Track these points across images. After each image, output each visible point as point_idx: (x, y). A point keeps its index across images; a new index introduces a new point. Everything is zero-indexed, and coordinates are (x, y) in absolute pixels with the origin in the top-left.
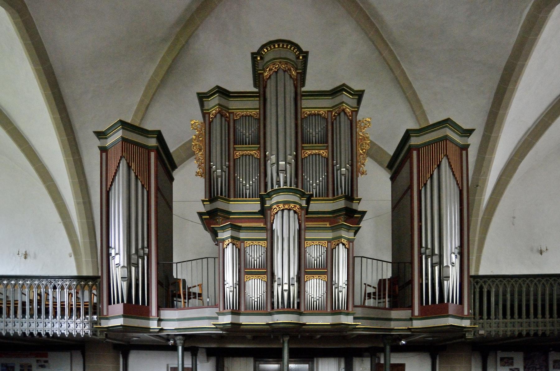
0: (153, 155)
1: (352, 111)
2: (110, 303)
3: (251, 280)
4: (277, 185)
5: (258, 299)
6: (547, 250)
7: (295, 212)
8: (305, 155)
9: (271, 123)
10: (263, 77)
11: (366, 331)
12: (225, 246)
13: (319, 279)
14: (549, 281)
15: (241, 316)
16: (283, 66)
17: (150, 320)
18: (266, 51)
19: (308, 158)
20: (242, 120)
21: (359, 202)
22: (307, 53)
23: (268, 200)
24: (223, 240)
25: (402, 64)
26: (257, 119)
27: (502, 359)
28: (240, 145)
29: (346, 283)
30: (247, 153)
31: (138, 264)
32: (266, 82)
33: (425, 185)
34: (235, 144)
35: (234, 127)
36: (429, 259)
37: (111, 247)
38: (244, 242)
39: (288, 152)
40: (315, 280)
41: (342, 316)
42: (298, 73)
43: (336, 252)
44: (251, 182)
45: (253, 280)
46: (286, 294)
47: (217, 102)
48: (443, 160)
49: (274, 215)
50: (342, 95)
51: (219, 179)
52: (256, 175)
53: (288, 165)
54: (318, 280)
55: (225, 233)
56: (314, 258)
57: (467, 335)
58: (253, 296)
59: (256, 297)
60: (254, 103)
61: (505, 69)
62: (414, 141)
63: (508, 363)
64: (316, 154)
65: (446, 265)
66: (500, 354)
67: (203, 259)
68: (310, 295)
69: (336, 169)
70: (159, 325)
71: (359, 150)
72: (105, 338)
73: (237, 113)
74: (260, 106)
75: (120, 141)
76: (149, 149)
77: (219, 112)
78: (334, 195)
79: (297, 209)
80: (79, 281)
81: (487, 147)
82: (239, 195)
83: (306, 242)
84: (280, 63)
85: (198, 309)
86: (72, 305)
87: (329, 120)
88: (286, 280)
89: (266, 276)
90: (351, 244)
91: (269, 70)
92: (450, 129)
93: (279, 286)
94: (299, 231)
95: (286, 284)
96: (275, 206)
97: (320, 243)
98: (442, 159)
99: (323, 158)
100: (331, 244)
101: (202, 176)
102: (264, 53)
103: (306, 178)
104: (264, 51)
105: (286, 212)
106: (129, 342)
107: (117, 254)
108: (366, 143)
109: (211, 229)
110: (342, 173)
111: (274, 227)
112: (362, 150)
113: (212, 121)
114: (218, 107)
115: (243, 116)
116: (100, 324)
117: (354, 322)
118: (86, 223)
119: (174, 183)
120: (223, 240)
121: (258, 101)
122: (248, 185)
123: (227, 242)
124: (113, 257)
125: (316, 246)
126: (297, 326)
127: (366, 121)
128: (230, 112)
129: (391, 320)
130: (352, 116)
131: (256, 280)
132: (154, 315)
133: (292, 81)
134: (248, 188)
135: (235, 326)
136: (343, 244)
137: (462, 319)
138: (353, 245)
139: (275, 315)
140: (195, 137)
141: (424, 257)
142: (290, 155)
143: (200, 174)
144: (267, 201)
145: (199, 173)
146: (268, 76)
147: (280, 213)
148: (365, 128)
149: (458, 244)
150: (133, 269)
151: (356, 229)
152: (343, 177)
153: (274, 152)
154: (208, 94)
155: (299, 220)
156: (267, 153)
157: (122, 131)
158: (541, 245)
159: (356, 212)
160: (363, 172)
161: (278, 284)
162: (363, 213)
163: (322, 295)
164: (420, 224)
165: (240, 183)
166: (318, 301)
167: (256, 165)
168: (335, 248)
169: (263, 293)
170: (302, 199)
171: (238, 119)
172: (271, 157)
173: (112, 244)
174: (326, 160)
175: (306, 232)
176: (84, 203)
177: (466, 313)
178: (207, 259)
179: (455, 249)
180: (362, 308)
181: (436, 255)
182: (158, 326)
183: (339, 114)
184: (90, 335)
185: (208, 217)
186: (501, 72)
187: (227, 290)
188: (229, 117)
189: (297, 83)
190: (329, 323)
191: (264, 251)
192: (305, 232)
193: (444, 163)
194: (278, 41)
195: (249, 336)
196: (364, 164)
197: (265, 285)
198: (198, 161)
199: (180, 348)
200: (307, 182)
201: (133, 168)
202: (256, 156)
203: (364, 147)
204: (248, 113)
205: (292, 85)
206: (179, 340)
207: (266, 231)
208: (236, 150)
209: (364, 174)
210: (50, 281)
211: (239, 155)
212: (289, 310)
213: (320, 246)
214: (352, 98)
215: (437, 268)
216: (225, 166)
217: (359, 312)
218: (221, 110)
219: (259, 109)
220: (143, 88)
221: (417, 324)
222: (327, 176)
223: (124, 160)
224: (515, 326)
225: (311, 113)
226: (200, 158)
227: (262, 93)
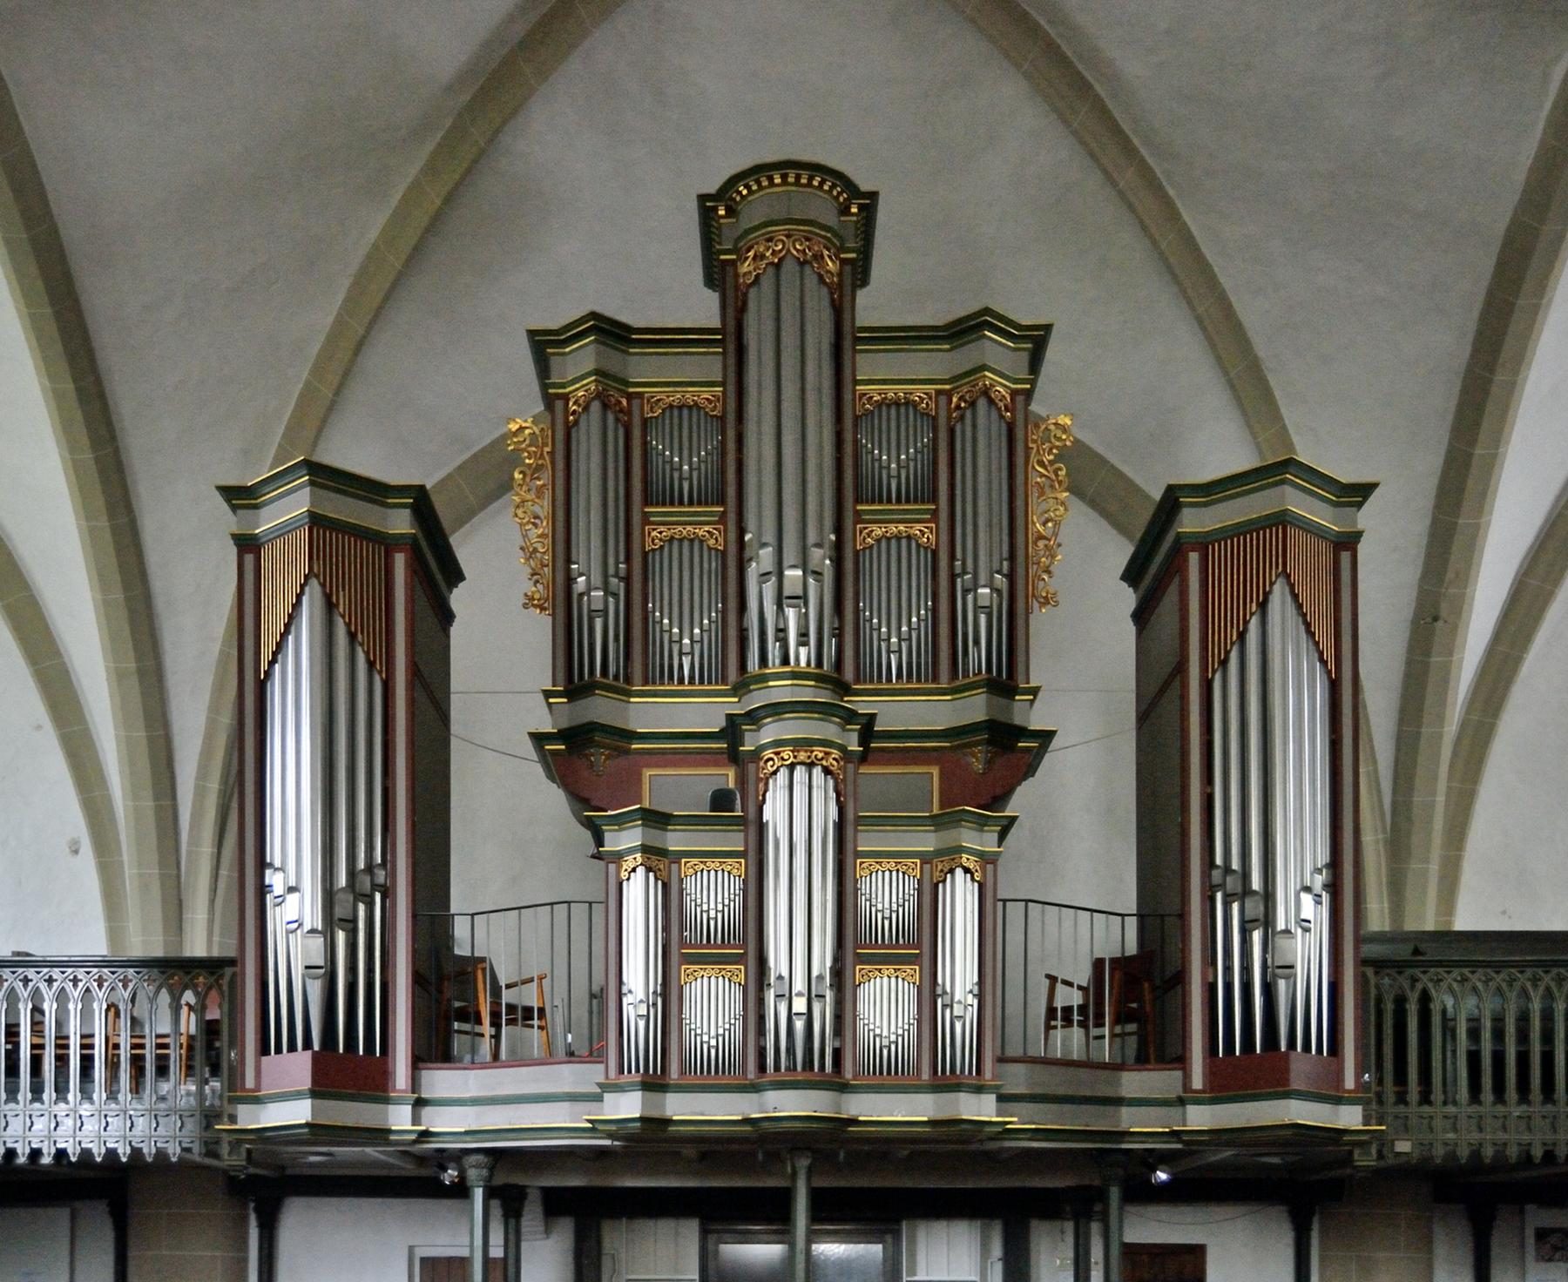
0: (400, 560)
1: (1014, 393)
2: (264, 1050)
3: (699, 980)
4: (778, 644)
5: (720, 1039)
8: (864, 539)
9: (760, 433)
10: (737, 275)
11: (1065, 1141)
12: (624, 875)
13: (897, 977)
15: (668, 1095)
16: (798, 247)
18: (745, 192)
19: (875, 548)
21: (1031, 697)
22: (873, 196)
23: (750, 730)
24: (618, 857)
25: (1182, 210)
26: (716, 416)
27: (1542, 1235)
28: (664, 505)
29: (976, 992)
30: (685, 532)
31: (354, 921)
32: (745, 295)
33: (1224, 663)
34: (647, 502)
35: (645, 444)
36: (1235, 906)
37: (271, 865)
39: (812, 537)
40: (886, 979)
41: (962, 1094)
42: (844, 262)
43: (945, 891)
44: (697, 631)
45: (705, 979)
46: (799, 1025)
47: (591, 366)
48: (1277, 588)
49: (767, 779)
50: (979, 343)
51: (598, 623)
52: (713, 609)
53: (811, 581)
54: (893, 980)
55: (624, 833)
56: (883, 911)
57: (1356, 1157)
58: (705, 1030)
59: (713, 1033)
60: (709, 365)
61: (1508, 242)
62: (1192, 521)
64: (898, 538)
65: (1283, 927)
66: (1538, 1218)
67: (555, 906)
68: (872, 1027)
69: (963, 586)
70: (416, 1120)
71: (1034, 523)
72: (244, 1163)
73: (653, 397)
74: (725, 376)
75: (306, 524)
76: (387, 544)
78: (954, 674)
79: (835, 763)
80: (166, 976)
81: (1461, 490)
82: (659, 675)
83: (858, 861)
84: (788, 236)
86: (117, 1046)
87: (942, 421)
88: (799, 984)
90: (990, 867)
92: (1297, 486)
93: (781, 1002)
94: (840, 826)
95: (799, 994)
96: (768, 754)
97: (899, 866)
98: (1272, 584)
99: (922, 550)
100: (932, 867)
101: (543, 609)
102: (738, 198)
103: (867, 618)
104: (740, 193)
105: (800, 773)
106: (283, 1168)
107: (291, 890)
109: (583, 819)
111: (767, 815)
113: (576, 422)
114: (595, 381)
115: (671, 406)
116: (233, 1119)
117: (997, 1116)
118: (145, 742)
119: (455, 631)
120: (618, 857)
121: (720, 358)
122: (686, 641)
123: (629, 863)
124: (276, 897)
125: (887, 873)
126: (831, 1125)
129: (1119, 1102)
131: (713, 979)
132: (404, 1087)
133: (825, 291)
135: (654, 1125)
136: (967, 870)
137: (1337, 1104)
139: (770, 1093)
140: (521, 476)
141: (1219, 896)
142: (819, 545)
143: (536, 602)
144: (746, 733)
145: (534, 600)
146: (753, 278)
147: (782, 776)
149: (1323, 857)
150: (341, 937)
151: (1005, 822)
152: (983, 619)
153: (769, 536)
154: (562, 334)
155: (838, 795)
156: (748, 537)
157: (311, 490)
159: (1023, 733)
160: (1046, 598)
161: (777, 996)
162: (1046, 736)
163: (906, 1027)
164: (1209, 791)
165: (662, 631)
166: (893, 1047)
168: (944, 881)
169: (733, 1021)
170: (848, 727)
171: (656, 418)
172: (761, 552)
173: (274, 854)
174: (929, 556)
175: (862, 831)
176: (141, 673)
177: (1350, 1083)
178: (566, 905)
179: (1312, 874)
180: (1029, 1065)
181: (1255, 893)
182: (413, 1125)
183: (973, 404)
184: (200, 1154)
185: (563, 747)
186: (1495, 248)
187: (629, 1012)
188: (629, 413)
189: (841, 296)
190: (925, 1119)
191: (737, 892)
192: (856, 831)
193: (1279, 597)
194: (784, 166)
195: (689, 1151)
196: (1051, 568)
197: (739, 996)
198: (531, 557)
199: (478, 1194)
200: (872, 629)
201: (341, 610)
202: (712, 542)
205: (826, 302)
206: (474, 1166)
207: (742, 828)
209: (1049, 603)
211: (661, 540)
212: (808, 1076)
213: (901, 875)
214: (1015, 350)
215: (1257, 936)
216: (616, 575)
217: (1018, 1079)
218: (603, 389)
219: (723, 384)
220: (345, 283)
221: (1200, 1118)
222: (935, 610)
223: (314, 582)
225: (886, 398)
226: (539, 546)
227: (731, 328)
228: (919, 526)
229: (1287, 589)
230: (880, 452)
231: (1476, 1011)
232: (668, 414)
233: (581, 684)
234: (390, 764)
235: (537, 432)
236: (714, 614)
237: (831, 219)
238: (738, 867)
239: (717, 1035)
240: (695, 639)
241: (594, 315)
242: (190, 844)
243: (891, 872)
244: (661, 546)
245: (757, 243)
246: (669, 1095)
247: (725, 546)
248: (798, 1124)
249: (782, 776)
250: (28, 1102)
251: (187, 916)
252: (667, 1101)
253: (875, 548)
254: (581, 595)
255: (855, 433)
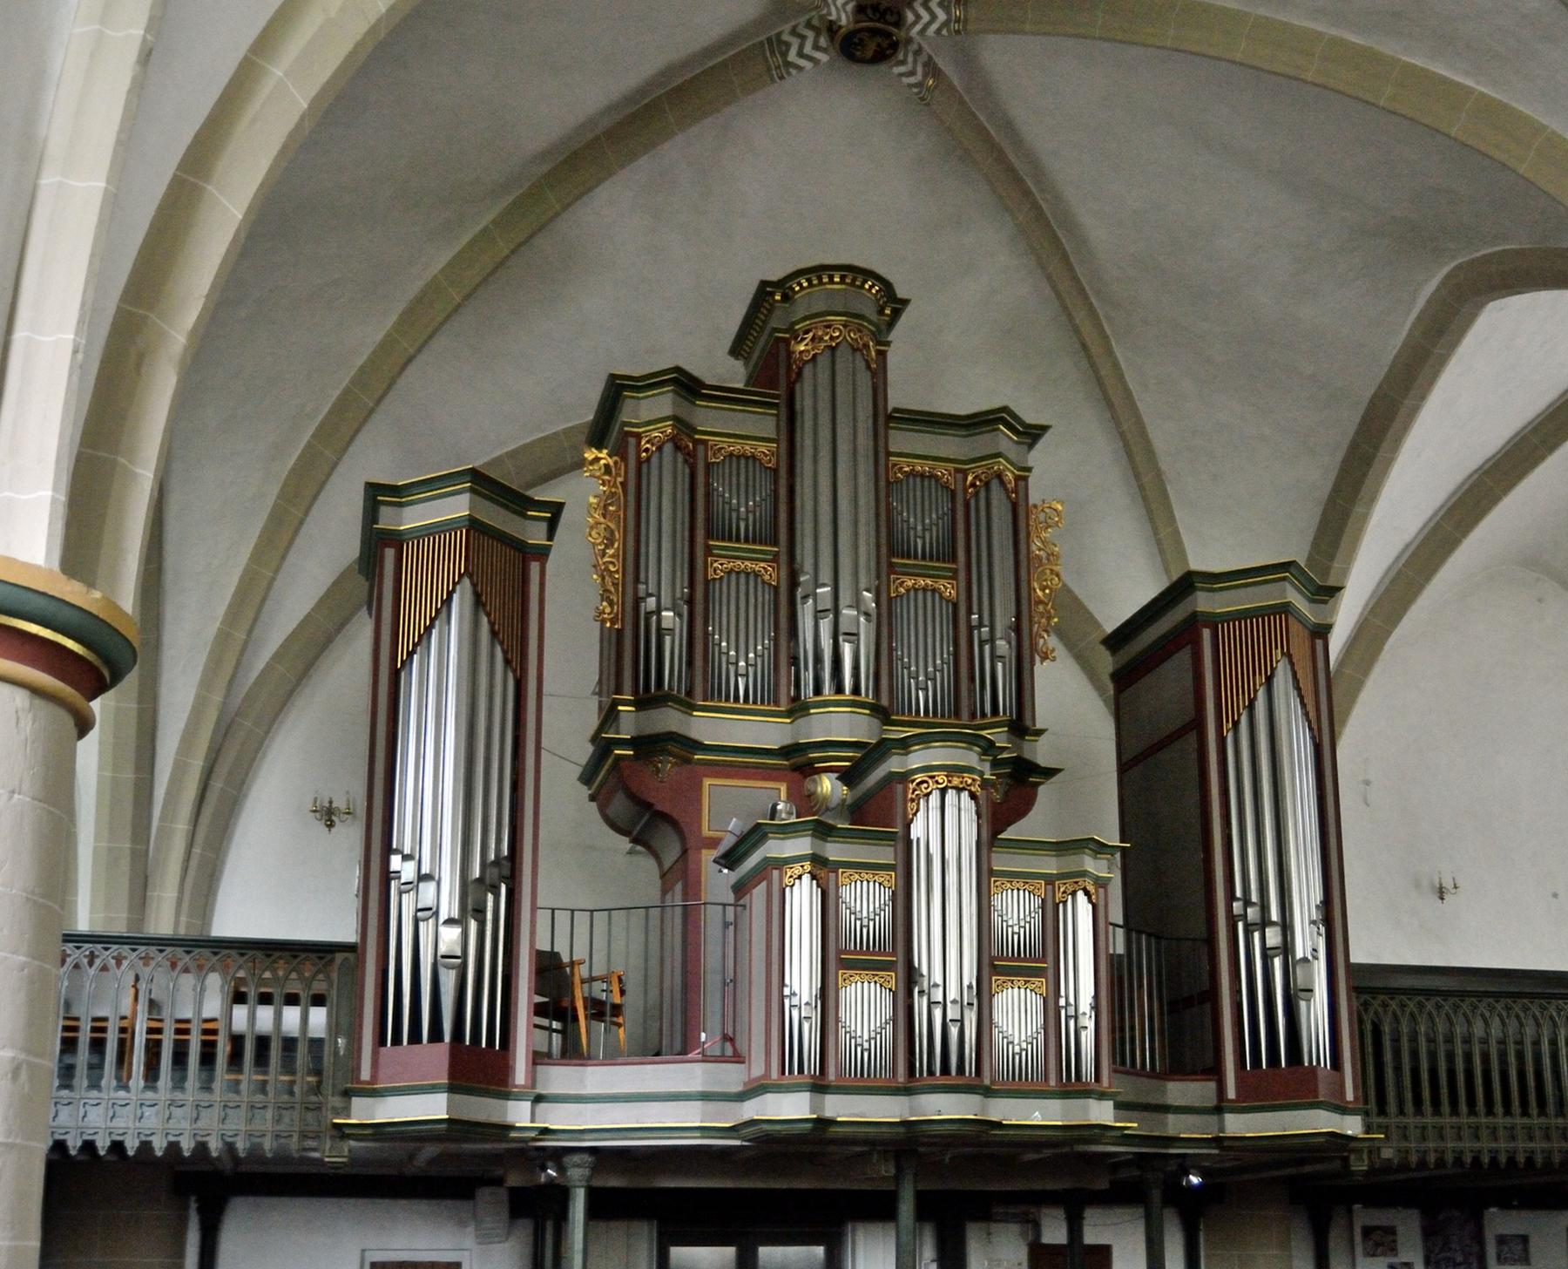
5: (873, 1042)
6: (1456, 887)
7: (973, 796)
14: (1529, 1009)
17: (508, 1099)
20: (727, 466)
26: (770, 468)
27: (1367, 1232)
30: (743, 566)
33: (1236, 724)
34: (709, 535)
35: (707, 485)
36: (1257, 935)
38: (837, 872)
39: (863, 583)
40: (1016, 990)
45: (859, 984)
47: (668, 412)
52: (766, 637)
62: (1205, 602)
63: (1383, 1244)
64: (925, 590)
66: (1363, 1217)
71: (1035, 590)
75: (464, 527)
77: (673, 439)
82: (716, 693)
83: (993, 879)
84: (845, 326)
85: (667, 1066)
89: (893, 974)
91: (813, 339)
98: (1277, 662)
100: (1054, 887)
102: (797, 289)
107: (423, 878)
108: (1052, 570)
110: (999, 653)
112: (1043, 589)
115: (731, 455)
122: (742, 664)
125: (1015, 891)
127: (1050, 508)
128: (698, 439)
129: (1166, 1109)
130: (1016, 491)
134: (744, 672)
136: (1087, 893)
138: (1106, 892)
141: (1240, 925)
148: (1050, 527)
153: (826, 574)
158: (1440, 872)
167: (767, 601)
171: (718, 463)
173: (404, 837)
177: (1350, 1096)
182: (532, 1122)
183: (987, 485)
185: (632, 753)
202: (767, 577)
203: (1046, 580)
204: (747, 448)
208: (713, 555)
210: (143, 955)
220: (400, 307)
221: (1238, 1125)
222: (956, 654)
224: (1480, 1135)
228: (943, 581)
229: (1289, 667)
230: (730, 494)
231: (1519, 1036)
232: (727, 461)
233: (645, 696)
234: (131, 731)
235: (611, 463)
236: (766, 642)
237: (874, 317)
238: (890, 878)
239: (870, 1039)
240: (750, 662)
241: (677, 369)
242: (163, 818)
243: (868, 882)
244: (722, 577)
245: (816, 328)
246: (828, 1097)
247: (778, 582)
248: (955, 1127)
249: (934, 799)
250: (54, 1089)
251: (153, 894)
252: (826, 1102)
253: (725, 580)
254: (649, 614)
255: (888, 496)
